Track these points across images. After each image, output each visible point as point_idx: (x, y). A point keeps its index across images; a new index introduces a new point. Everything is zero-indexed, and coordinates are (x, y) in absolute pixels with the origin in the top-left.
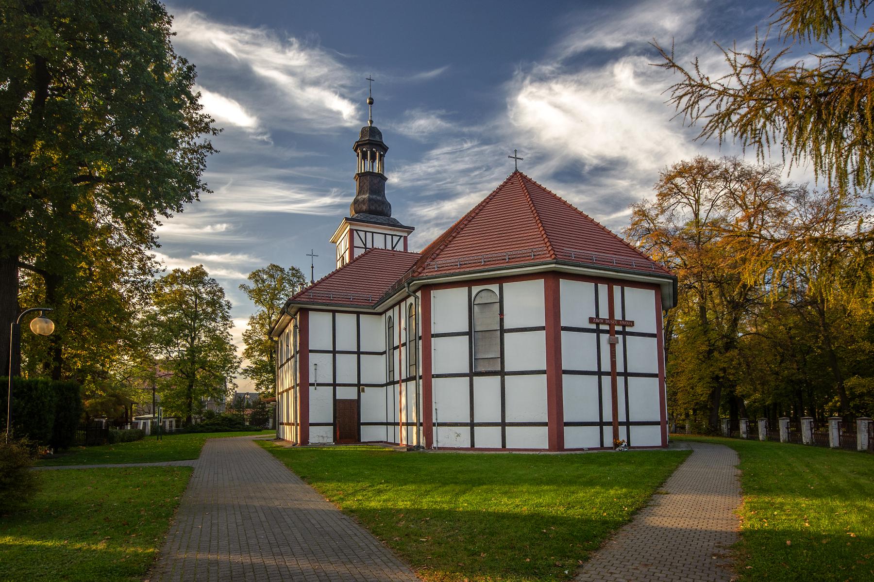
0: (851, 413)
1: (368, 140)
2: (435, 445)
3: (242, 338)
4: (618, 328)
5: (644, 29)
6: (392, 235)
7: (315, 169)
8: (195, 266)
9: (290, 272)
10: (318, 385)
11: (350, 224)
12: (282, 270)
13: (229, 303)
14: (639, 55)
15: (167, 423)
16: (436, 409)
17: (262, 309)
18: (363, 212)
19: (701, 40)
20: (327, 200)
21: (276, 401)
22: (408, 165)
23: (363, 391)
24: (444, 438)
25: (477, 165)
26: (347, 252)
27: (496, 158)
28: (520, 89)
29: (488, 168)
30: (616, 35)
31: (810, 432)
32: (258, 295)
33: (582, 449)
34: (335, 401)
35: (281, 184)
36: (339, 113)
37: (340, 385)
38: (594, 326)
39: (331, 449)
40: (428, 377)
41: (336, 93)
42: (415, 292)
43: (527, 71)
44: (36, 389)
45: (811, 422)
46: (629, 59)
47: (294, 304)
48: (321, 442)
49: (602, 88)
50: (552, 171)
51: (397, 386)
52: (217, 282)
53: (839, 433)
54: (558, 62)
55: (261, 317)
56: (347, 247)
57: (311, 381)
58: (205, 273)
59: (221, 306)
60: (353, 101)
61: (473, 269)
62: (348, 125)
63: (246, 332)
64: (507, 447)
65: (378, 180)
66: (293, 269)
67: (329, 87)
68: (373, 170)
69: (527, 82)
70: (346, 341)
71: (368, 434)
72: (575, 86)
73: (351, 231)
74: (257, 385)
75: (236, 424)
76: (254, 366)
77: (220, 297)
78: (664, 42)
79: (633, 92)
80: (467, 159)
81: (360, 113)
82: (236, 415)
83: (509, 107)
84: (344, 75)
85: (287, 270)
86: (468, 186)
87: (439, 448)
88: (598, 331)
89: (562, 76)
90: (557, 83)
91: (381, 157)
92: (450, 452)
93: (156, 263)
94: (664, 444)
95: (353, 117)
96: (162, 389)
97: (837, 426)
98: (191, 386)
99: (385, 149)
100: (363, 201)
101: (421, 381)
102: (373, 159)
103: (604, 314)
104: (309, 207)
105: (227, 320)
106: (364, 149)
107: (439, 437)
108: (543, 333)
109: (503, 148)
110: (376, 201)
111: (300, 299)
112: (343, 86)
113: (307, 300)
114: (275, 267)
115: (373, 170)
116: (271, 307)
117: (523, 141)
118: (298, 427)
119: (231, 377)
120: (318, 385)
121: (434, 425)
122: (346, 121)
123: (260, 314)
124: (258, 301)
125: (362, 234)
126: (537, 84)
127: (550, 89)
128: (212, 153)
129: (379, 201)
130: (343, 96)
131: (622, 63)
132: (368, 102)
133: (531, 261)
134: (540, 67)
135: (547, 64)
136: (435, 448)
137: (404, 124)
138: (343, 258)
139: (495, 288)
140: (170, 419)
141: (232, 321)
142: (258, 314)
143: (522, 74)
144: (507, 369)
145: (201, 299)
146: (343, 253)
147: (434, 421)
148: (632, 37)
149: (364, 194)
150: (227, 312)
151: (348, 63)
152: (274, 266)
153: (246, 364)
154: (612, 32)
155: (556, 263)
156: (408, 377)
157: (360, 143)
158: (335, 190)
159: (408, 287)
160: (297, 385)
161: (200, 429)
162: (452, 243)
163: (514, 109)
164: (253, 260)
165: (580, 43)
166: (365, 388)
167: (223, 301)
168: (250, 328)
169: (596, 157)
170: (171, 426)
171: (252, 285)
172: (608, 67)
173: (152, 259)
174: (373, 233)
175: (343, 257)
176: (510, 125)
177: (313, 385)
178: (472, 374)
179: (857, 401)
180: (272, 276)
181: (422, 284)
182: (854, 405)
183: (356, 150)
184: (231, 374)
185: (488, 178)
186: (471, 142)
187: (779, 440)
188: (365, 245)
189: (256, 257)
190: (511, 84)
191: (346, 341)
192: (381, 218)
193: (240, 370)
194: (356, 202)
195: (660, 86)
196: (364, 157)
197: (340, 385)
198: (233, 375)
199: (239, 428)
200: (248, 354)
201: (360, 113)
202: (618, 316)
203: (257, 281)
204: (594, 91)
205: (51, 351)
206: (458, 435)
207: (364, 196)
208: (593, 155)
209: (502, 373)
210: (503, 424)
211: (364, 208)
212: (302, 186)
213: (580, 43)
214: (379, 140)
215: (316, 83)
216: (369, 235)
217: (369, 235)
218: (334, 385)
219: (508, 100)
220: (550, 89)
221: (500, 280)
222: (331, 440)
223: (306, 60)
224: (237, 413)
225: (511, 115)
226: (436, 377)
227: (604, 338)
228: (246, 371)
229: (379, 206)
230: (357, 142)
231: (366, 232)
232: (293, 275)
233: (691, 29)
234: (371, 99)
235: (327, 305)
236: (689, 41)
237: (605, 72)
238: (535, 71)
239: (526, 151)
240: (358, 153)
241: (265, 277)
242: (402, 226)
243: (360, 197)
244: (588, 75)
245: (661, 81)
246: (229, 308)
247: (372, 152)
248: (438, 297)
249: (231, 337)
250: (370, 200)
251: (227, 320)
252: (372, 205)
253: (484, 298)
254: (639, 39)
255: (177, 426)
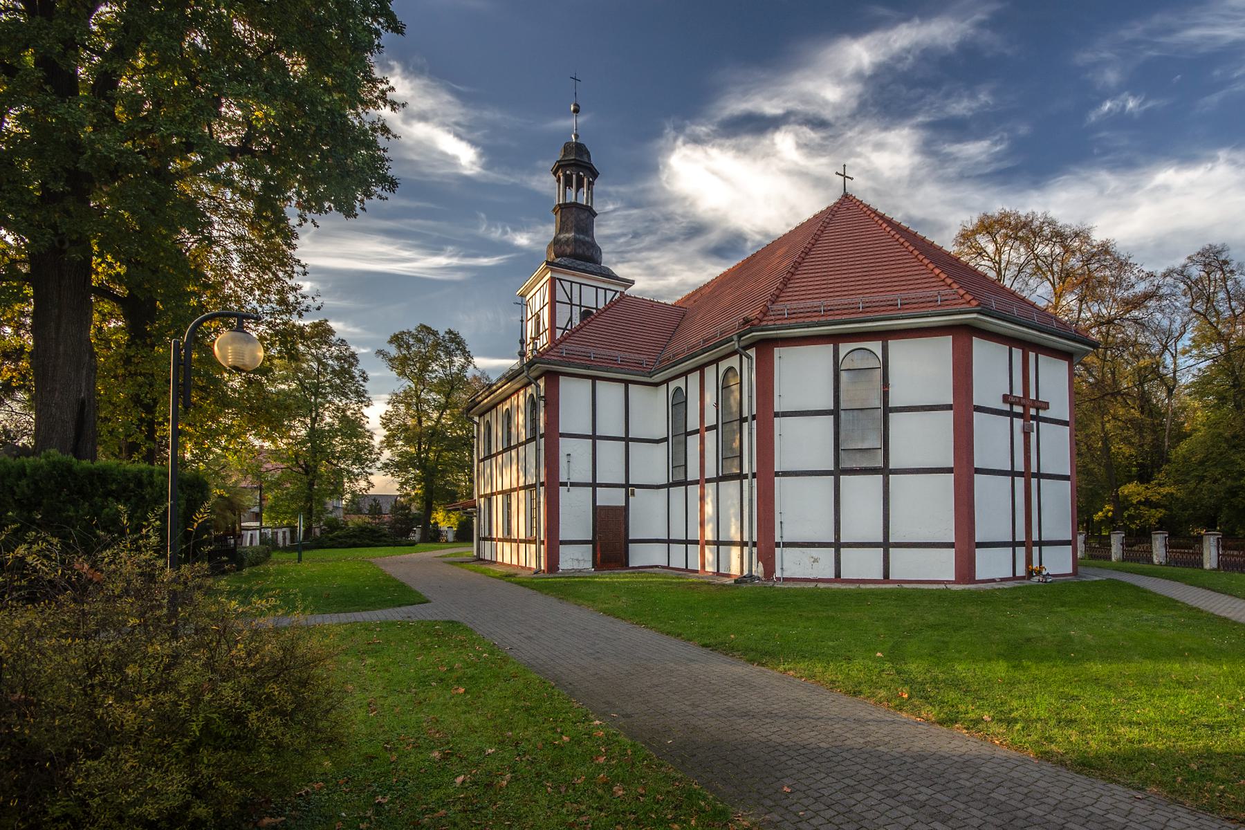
0: (1125, 524)
1: (575, 159)
2: (778, 574)
3: (379, 421)
4: (1033, 412)
5: (806, 99)
6: (606, 289)
7: (431, 223)
8: (317, 321)
9: (447, 336)
10: (573, 484)
11: (552, 270)
12: (435, 333)
13: (364, 373)
14: (800, 124)
15: (280, 535)
16: (781, 523)
17: (407, 383)
18: (566, 256)
19: (865, 116)
20: (442, 261)
21: (475, 507)
22: (543, 225)
23: (633, 494)
24: (792, 564)
25: (625, 230)
26: (546, 308)
27: (647, 224)
28: (672, 150)
29: (636, 235)
30: (775, 102)
31: (1164, 549)
32: (400, 364)
33: (993, 581)
34: (595, 507)
35: (380, 238)
36: (455, 158)
37: (601, 485)
38: (1007, 407)
39: (607, 580)
40: (766, 475)
41: (449, 132)
42: (746, 348)
43: (679, 129)
44: (151, 484)
45: (1166, 537)
46: (791, 128)
47: (542, 363)
48: (575, 567)
49: (763, 157)
50: (713, 245)
51: (694, 491)
52: (349, 344)
53: (1218, 551)
54: (713, 125)
55: (406, 393)
56: (546, 301)
57: (563, 479)
58: (331, 332)
59: (353, 378)
60: (473, 143)
61: (839, 317)
62: (468, 172)
63: (386, 414)
64: (843, 576)
65: (586, 214)
66: (450, 332)
67: (443, 125)
68: (576, 199)
69: (680, 142)
70: (610, 423)
71: (640, 556)
72: (734, 151)
73: (553, 280)
74: (402, 484)
75: (381, 536)
76: (397, 459)
77: (351, 365)
78: (827, 114)
79: (796, 164)
80: (613, 223)
81: (484, 159)
82: (369, 523)
83: (661, 167)
84: (457, 112)
85: (441, 333)
86: (614, 255)
87: (786, 580)
88: (1012, 414)
89: (719, 141)
90: (713, 146)
91: (590, 184)
92: (803, 585)
93: (304, 297)
94: (1075, 573)
95: (473, 163)
96: (270, 489)
97: (1215, 543)
98: (311, 484)
99: (595, 174)
100: (567, 242)
101: (755, 480)
102: (580, 185)
103: (1018, 392)
104: (422, 268)
105: (363, 396)
106: (568, 172)
107: (784, 564)
108: (950, 414)
109: (654, 213)
110: (584, 243)
111: (547, 357)
112: (457, 124)
113: (558, 358)
114: (427, 330)
115: (576, 199)
116: (420, 379)
117: (677, 209)
118: (542, 546)
119: (367, 473)
120: (573, 484)
121: (778, 545)
122: (466, 168)
123: (405, 391)
124: (402, 373)
125: (567, 285)
126: (689, 146)
127: (706, 152)
128: (389, 138)
129: (588, 242)
130: (459, 136)
131: (783, 132)
132: (572, 109)
133: (938, 309)
134: (693, 127)
135: (703, 125)
136: (778, 579)
137: (536, 178)
138: (539, 317)
139: (876, 346)
140: (284, 529)
141: (369, 398)
142: (401, 390)
143: (673, 133)
144: (892, 465)
145: (325, 366)
146: (538, 309)
147: (777, 539)
148: (791, 105)
149: (567, 232)
150: (361, 385)
151: (463, 98)
152: (425, 326)
153: (387, 454)
154: (771, 98)
155: (979, 312)
156: (720, 475)
157: (563, 163)
158: (450, 248)
159: (739, 341)
160: (542, 484)
161: (330, 543)
162: (792, 281)
163: (666, 171)
164: (350, 329)
165: (737, 106)
166: (636, 490)
167: (356, 371)
168: (390, 408)
169: (759, 233)
170: (284, 539)
171: (393, 351)
172: (769, 136)
173: (298, 291)
174: (581, 284)
175: (538, 316)
176: (663, 189)
177: (564, 484)
178: (838, 472)
179: (1132, 511)
180: (419, 340)
181: (761, 337)
182: (1129, 515)
183: (555, 173)
184: (366, 469)
185: (637, 247)
186: (614, 204)
187: (1110, 558)
188: (571, 300)
189: (356, 326)
190: (661, 143)
191: (610, 423)
192: (591, 266)
193: (379, 464)
194: (556, 241)
195: (824, 160)
196: (568, 183)
197: (601, 485)
198: (369, 471)
199: (385, 541)
200: (389, 442)
201: (484, 159)
202: (1033, 396)
203: (400, 346)
204: (755, 159)
205: (142, 425)
206: (816, 561)
207: (567, 235)
208: (754, 229)
209: (885, 471)
210: (886, 545)
211: (568, 250)
212: (410, 242)
213: (737, 106)
214: (587, 160)
215: (423, 117)
216: (576, 287)
217: (576, 287)
218: (594, 485)
219: (660, 159)
220: (706, 152)
221: (884, 336)
222: (588, 565)
223: (412, 89)
224: (370, 520)
225: (664, 177)
226: (782, 476)
227: (1018, 423)
228: (386, 465)
229: (588, 249)
230: (558, 161)
231: (572, 282)
232: (452, 340)
233: (853, 104)
234: (576, 105)
235: (588, 368)
236: (853, 116)
237: (766, 141)
238: (688, 131)
239: (681, 220)
240: (559, 176)
241: (412, 341)
242: (617, 278)
243: (562, 236)
244: (746, 140)
245: (824, 156)
246: (365, 379)
247: (578, 175)
248: (787, 362)
249: (367, 420)
250: (576, 240)
251: (363, 396)
252: (580, 247)
253: (859, 361)
254: (800, 107)
255: (292, 539)
